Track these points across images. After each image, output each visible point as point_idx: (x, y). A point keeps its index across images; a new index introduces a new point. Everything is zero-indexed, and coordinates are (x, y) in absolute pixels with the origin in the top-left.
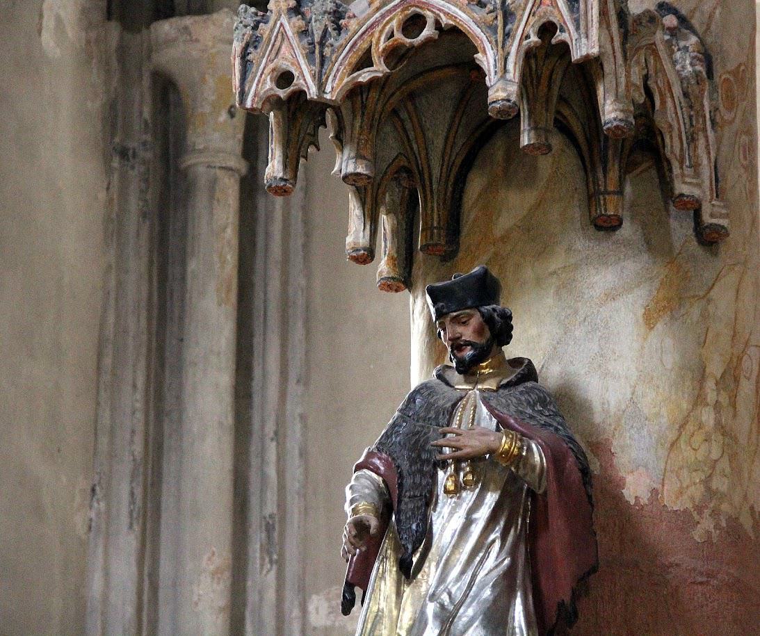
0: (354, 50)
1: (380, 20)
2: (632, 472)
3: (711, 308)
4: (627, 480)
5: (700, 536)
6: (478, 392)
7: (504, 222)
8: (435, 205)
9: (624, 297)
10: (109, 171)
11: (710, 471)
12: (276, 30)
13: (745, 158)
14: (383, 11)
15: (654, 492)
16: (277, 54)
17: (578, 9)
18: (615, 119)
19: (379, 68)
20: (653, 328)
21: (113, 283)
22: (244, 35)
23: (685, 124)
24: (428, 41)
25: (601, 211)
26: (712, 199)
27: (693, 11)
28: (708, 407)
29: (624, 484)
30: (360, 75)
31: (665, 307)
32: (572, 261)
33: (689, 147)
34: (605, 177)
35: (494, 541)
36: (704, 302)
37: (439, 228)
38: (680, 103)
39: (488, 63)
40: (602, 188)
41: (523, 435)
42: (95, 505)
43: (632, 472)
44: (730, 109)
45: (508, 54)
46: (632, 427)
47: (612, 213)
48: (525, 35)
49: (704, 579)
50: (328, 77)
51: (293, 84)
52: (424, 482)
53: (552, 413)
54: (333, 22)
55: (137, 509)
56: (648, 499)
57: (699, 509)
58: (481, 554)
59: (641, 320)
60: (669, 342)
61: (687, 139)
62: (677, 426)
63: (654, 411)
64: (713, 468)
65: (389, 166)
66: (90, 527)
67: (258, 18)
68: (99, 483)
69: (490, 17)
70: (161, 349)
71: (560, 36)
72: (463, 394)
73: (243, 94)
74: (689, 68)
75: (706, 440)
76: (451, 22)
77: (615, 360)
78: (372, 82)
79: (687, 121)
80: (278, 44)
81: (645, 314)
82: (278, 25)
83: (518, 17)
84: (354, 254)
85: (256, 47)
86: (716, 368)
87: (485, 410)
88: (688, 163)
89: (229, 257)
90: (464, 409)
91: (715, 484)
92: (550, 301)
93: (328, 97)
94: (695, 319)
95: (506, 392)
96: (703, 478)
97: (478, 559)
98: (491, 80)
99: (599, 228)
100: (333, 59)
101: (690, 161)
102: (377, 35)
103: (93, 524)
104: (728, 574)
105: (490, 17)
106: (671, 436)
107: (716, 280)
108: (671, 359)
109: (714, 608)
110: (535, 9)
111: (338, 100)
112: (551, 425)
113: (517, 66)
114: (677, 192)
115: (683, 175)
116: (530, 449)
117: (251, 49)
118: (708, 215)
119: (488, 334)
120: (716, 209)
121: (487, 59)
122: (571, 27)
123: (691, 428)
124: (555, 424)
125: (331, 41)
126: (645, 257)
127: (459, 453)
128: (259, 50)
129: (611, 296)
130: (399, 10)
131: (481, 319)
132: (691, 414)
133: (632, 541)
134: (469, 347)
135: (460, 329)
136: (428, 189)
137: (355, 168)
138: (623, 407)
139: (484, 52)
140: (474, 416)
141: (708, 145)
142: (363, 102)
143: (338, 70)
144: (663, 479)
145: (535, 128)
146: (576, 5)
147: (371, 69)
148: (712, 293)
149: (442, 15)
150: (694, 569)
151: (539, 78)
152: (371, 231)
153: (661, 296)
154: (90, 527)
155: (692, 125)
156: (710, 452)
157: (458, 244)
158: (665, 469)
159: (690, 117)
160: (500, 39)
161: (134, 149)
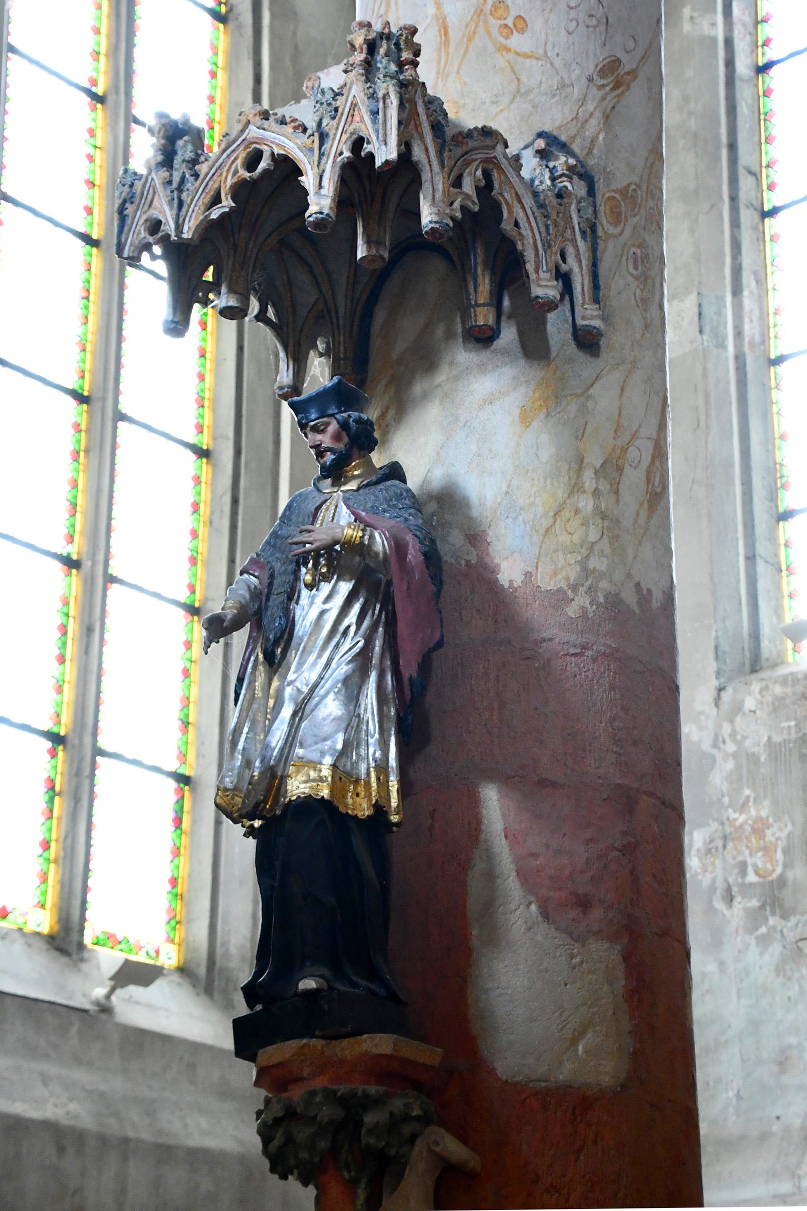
2: (507, 558)
3: (590, 404)
4: (502, 566)
5: (574, 612)
6: (341, 493)
7: (400, 346)
8: (342, 339)
9: (501, 400)
12: (148, 185)
13: (636, 268)
14: (228, 152)
15: (528, 575)
18: (431, 222)
19: (227, 203)
20: (528, 426)
22: (122, 193)
23: (540, 233)
24: (265, 171)
25: (472, 323)
26: (583, 304)
27: (574, 138)
28: (585, 496)
29: (499, 570)
30: (211, 213)
32: (454, 372)
34: (476, 291)
35: (349, 627)
36: (582, 399)
37: (345, 359)
38: (533, 213)
39: (309, 183)
41: (367, 525)
43: (507, 558)
44: (615, 224)
45: (324, 171)
48: (338, 152)
49: (579, 651)
53: (405, 506)
54: (191, 169)
57: (575, 588)
59: (517, 419)
60: (545, 437)
61: (543, 245)
62: (552, 514)
63: (528, 501)
65: (309, 312)
69: (309, 141)
71: (367, 148)
72: (328, 496)
75: (583, 525)
76: (283, 152)
77: (492, 458)
78: (223, 216)
79: (543, 229)
80: (150, 197)
81: (521, 413)
82: (150, 180)
83: (331, 136)
86: (595, 458)
87: (344, 508)
88: (545, 268)
90: (327, 509)
91: (593, 563)
93: (185, 236)
94: (572, 415)
95: (366, 490)
96: (579, 558)
98: (311, 199)
99: (478, 340)
101: (547, 266)
102: (224, 174)
105: (309, 141)
106: (546, 523)
108: (547, 453)
110: (346, 127)
111: (195, 239)
113: (332, 181)
114: (533, 295)
115: (538, 279)
116: (372, 537)
118: (580, 318)
119: (346, 439)
121: (308, 181)
122: (374, 138)
123: (567, 514)
125: (189, 185)
126: (522, 362)
129: (489, 401)
131: (337, 426)
132: (568, 501)
133: (505, 621)
134: (329, 453)
135: (319, 437)
136: (335, 325)
137: (227, 302)
138: (499, 500)
140: (334, 514)
141: (579, 254)
142: (234, 242)
143: (193, 211)
144: (537, 563)
145: (369, 242)
148: (591, 391)
149: (274, 146)
150: (568, 643)
152: (294, 373)
153: (537, 395)
155: (548, 233)
156: (587, 535)
159: (547, 227)
160: (316, 158)
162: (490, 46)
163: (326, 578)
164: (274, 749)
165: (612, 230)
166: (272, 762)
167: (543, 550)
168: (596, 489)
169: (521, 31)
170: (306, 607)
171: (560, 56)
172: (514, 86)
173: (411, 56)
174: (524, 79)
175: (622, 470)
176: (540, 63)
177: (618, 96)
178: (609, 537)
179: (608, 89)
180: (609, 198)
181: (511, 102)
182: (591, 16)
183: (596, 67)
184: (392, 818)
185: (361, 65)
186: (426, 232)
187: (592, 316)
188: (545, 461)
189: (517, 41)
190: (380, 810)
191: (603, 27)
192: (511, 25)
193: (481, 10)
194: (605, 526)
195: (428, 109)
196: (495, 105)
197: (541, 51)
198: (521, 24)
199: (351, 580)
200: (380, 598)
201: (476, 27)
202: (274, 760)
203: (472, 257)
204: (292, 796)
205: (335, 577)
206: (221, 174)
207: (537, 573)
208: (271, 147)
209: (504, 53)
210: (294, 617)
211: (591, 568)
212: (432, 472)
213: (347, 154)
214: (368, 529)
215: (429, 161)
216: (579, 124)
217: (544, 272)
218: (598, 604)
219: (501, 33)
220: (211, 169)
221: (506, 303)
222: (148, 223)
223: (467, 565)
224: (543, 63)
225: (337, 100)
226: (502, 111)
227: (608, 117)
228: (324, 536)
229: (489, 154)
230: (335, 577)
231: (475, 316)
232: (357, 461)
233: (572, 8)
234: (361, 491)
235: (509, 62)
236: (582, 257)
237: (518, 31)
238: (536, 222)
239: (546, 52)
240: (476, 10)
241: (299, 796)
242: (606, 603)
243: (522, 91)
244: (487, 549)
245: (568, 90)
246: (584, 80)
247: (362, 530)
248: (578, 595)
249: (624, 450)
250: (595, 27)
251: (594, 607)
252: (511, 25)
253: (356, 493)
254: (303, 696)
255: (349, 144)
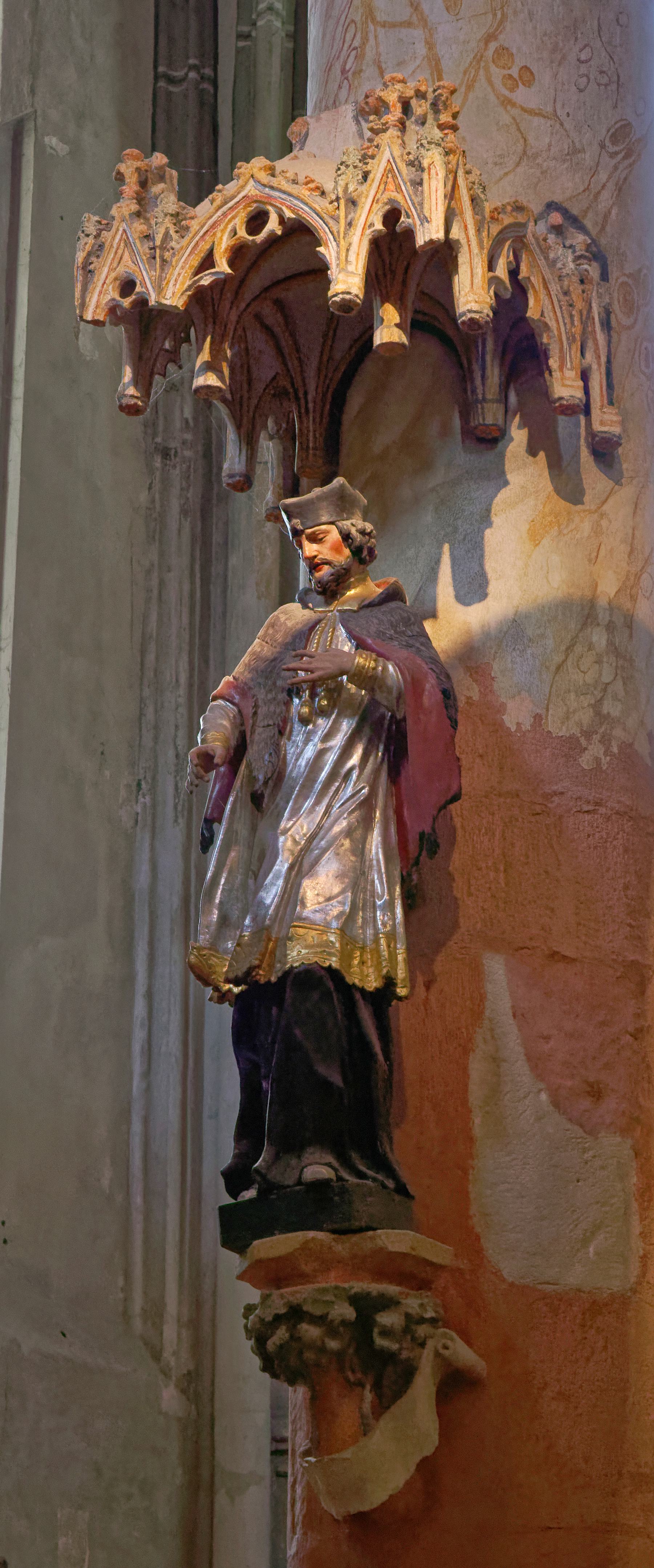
0: (196, 252)
1: (222, 219)
3: (604, 523)
4: (508, 705)
6: (337, 614)
10: (151, 471)
11: (602, 695)
13: (647, 366)
16: (119, 262)
17: (422, 192)
21: (155, 582)
23: (565, 324)
25: (478, 420)
26: (602, 406)
29: (505, 710)
30: (201, 278)
31: (551, 523)
33: (570, 348)
34: (483, 384)
35: (351, 769)
37: (315, 449)
40: (480, 397)
42: (141, 800)
45: (350, 244)
46: (514, 649)
47: (491, 423)
48: (368, 224)
49: (591, 808)
50: (169, 282)
51: (135, 292)
52: (278, 711)
55: (181, 803)
56: (531, 726)
57: (588, 734)
58: (337, 784)
61: (568, 339)
62: (563, 648)
64: (605, 690)
66: (137, 822)
67: (101, 227)
68: (145, 778)
70: (205, 646)
72: (323, 615)
73: (83, 305)
74: (572, 266)
75: (596, 662)
79: (567, 320)
80: (120, 252)
81: (529, 529)
84: (230, 481)
85: (98, 257)
89: (268, 551)
92: (428, 517)
94: (586, 534)
96: (593, 702)
97: (333, 788)
99: (481, 440)
100: (174, 263)
101: (571, 362)
102: (219, 235)
103: (139, 818)
104: (619, 802)
107: (610, 494)
109: (602, 838)
110: (379, 195)
112: (412, 646)
116: (385, 669)
117: (93, 259)
118: (598, 423)
120: (606, 417)
124: (418, 645)
125: (173, 244)
127: (315, 675)
128: (100, 260)
130: (242, 207)
132: (580, 635)
139: (327, 246)
143: (179, 274)
146: (420, 188)
147: (213, 270)
148: (605, 507)
149: (284, 208)
150: (580, 798)
151: (393, 272)
153: (547, 510)
154: (137, 822)
156: (601, 675)
157: (338, 464)
158: (550, 693)
161: (175, 449)
162: (492, 98)
163: (323, 713)
164: (270, 906)
165: (626, 321)
166: (267, 922)
167: (554, 690)
168: (610, 622)
169: (528, 84)
170: (300, 744)
171: (571, 117)
172: (520, 148)
173: (450, 119)
174: (531, 140)
175: (635, 601)
176: (549, 123)
177: (631, 165)
178: (623, 678)
179: (620, 156)
180: (623, 283)
181: (518, 164)
182: (602, 72)
183: (608, 131)
184: (398, 990)
185: (395, 126)
186: (463, 323)
187: (612, 421)
188: (556, 586)
189: (521, 95)
190: (389, 982)
191: (614, 87)
192: (516, 75)
193: (482, 57)
194: (619, 665)
195: (467, 179)
196: (497, 167)
197: (549, 109)
198: (527, 76)
199: (354, 715)
200: (383, 738)
201: (476, 76)
202: (270, 919)
203: (480, 344)
204: (293, 961)
205: (336, 711)
206: (214, 234)
207: (547, 716)
208: (281, 209)
209: (509, 108)
210: (285, 755)
211: (605, 712)
212: (425, 591)
213: (379, 226)
214: (381, 659)
215: (468, 241)
216: (591, 197)
217: (568, 370)
218: (613, 755)
219: (505, 85)
220: (202, 227)
221: (513, 398)
222: (118, 282)
223: (467, 703)
224: (552, 122)
225: (367, 164)
226: (506, 174)
227: (620, 190)
228: (328, 665)
229: (519, 232)
230: (336, 711)
231: (483, 413)
232: (357, 577)
233: (583, 62)
234: (362, 613)
235: (514, 118)
236: (601, 352)
237: (524, 84)
238: (561, 311)
239: (555, 111)
240: (476, 55)
241: (303, 963)
242: (619, 753)
243: (529, 153)
244: (491, 685)
245: (579, 155)
246: (596, 147)
247: (375, 661)
248: (591, 744)
249: (638, 577)
250: (606, 85)
251: (608, 758)
252: (516, 75)
253: (355, 615)
254: (299, 847)
255: (380, 214)
